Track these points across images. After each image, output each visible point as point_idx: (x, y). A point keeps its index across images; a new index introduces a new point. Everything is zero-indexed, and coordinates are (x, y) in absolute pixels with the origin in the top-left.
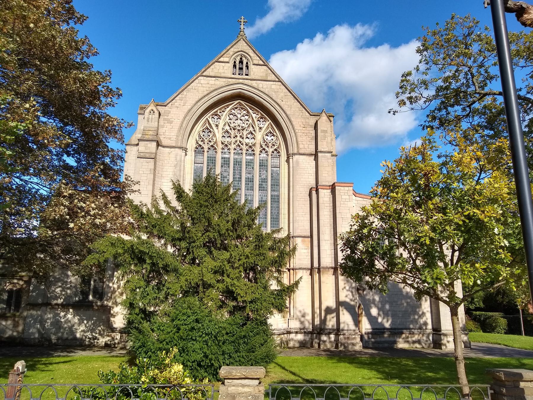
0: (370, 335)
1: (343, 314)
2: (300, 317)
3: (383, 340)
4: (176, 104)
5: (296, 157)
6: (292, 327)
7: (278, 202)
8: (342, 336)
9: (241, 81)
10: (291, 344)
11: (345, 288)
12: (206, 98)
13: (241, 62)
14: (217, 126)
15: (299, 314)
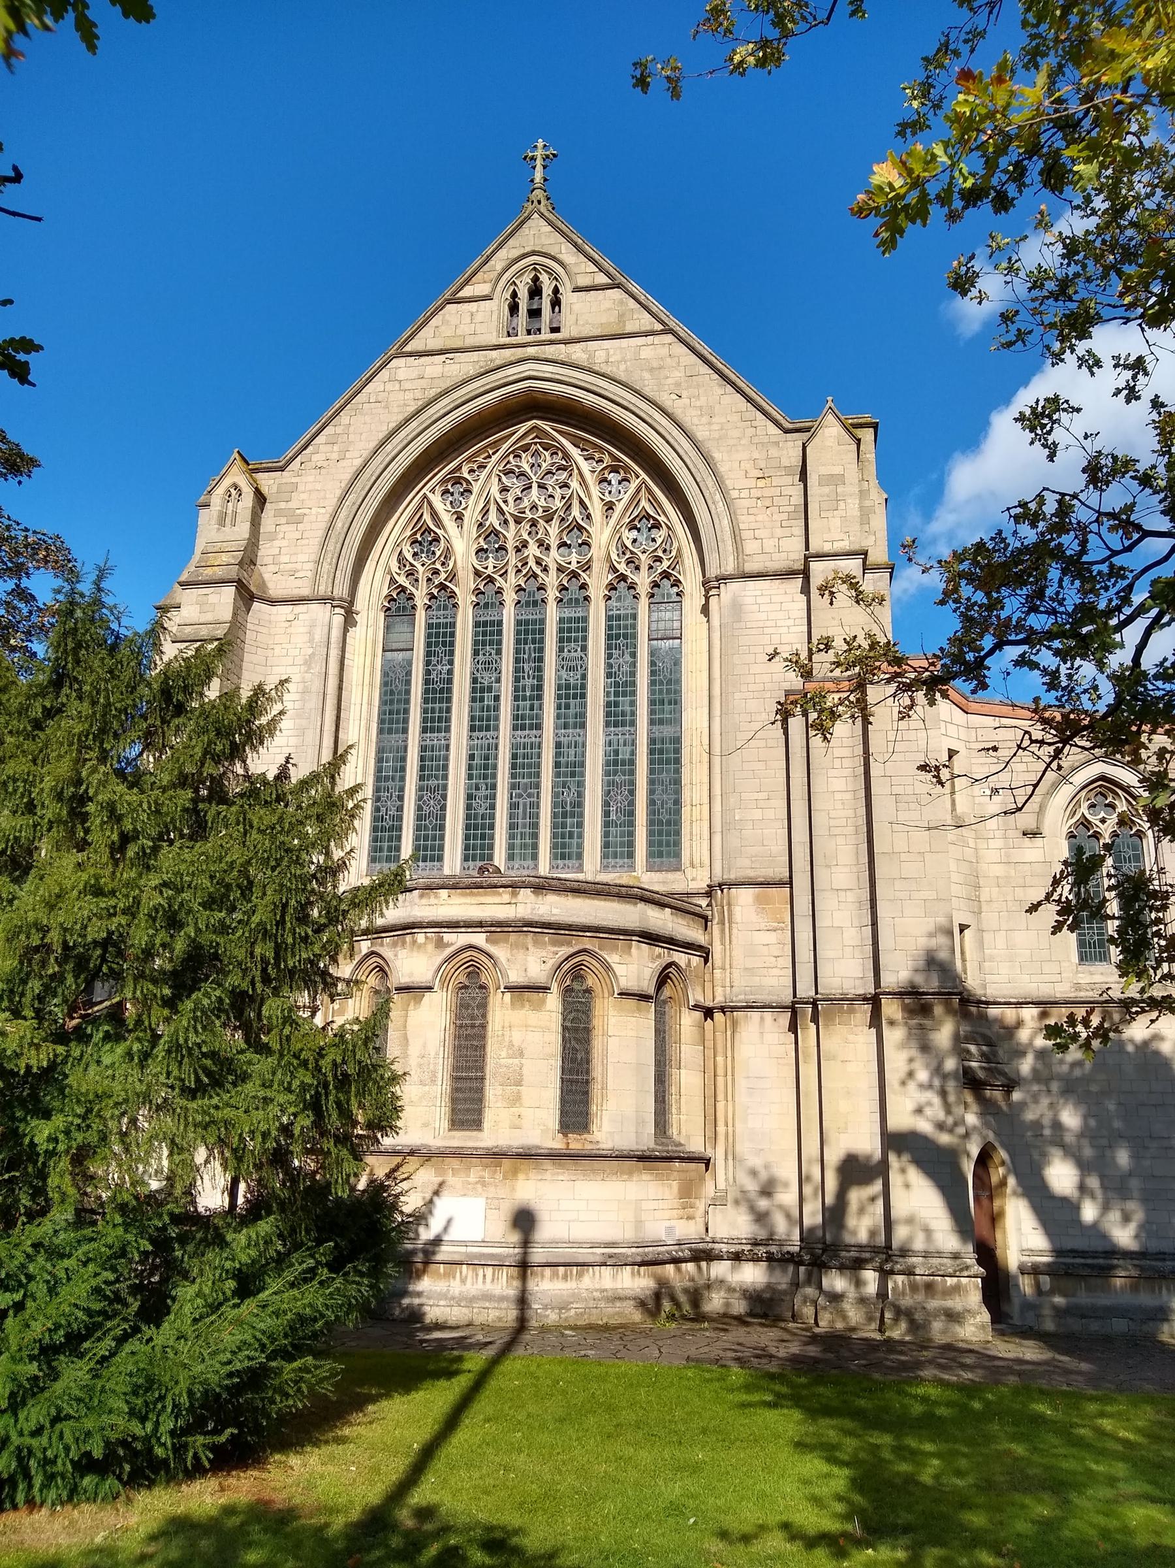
0: (1045, 1280)
1: (907, 1186)
2: (753, 1195)
3: (1103, 1300)
4: (315, 458)
5: (730, 590)
6: (719, 1236)
7: (678, 761)
8: (900, 1279)
9: (531, 351)
10: (715, 1302)
11: (911, 1074)
12: (414, 424)
13: (535, 291)
14: (459, 517)
15: (752, 1186)
